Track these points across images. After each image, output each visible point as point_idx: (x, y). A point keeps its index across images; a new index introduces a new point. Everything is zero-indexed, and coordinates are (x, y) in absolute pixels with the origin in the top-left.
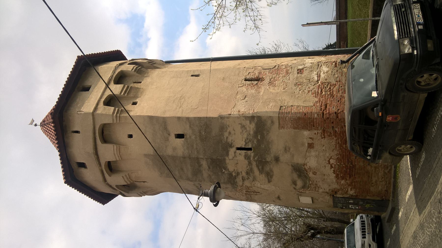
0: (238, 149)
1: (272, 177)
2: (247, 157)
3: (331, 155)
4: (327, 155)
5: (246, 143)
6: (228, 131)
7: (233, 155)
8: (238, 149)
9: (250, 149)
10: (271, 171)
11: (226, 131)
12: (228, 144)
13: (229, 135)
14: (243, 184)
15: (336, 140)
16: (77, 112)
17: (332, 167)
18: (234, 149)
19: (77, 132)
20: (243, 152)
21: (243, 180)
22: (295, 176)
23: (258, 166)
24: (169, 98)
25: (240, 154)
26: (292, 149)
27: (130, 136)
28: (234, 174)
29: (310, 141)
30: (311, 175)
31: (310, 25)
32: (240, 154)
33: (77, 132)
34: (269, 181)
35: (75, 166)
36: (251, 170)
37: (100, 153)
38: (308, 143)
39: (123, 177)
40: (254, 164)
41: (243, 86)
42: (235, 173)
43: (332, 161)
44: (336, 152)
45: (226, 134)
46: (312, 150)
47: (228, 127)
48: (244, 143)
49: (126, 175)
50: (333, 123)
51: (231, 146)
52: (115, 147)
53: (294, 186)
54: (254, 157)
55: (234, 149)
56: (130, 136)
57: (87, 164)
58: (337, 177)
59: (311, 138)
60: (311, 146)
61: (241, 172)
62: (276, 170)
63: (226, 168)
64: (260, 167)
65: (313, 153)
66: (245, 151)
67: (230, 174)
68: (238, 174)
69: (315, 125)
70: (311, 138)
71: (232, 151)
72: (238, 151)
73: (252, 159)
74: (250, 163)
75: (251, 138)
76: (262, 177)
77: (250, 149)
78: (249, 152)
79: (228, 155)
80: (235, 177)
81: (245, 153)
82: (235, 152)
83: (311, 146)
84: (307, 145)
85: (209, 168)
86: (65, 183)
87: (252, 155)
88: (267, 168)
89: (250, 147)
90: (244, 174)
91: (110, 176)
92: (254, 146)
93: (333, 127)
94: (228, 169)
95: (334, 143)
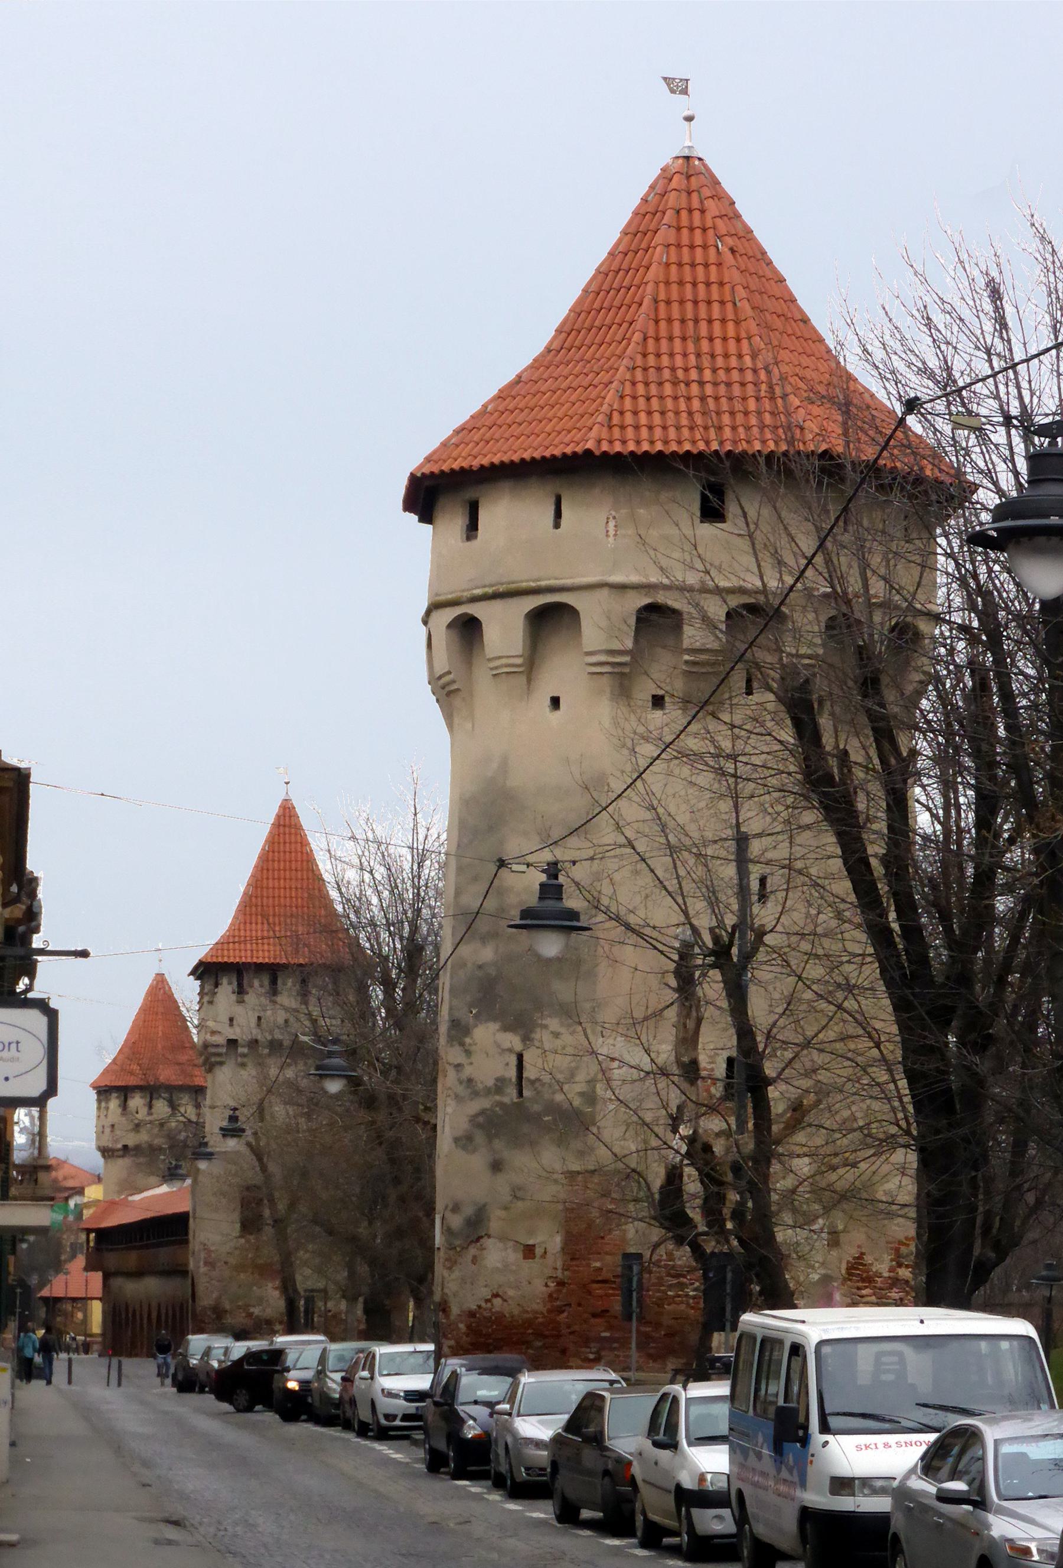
0: (520, 1057)
1: (464, 1148)
2: (500, 1084)
3: (510, 1302)
4: (511, 1293)
5: (532, 1082)
6: (562, 1030)
7: (507, 1045)
8: (520, 1057)
9: (520, 1094)
10: (474, 1151)
11: (562, 1024)
12: (531, 1032)
13: (552, 1032)
14: (450, 1064)
15: (542, 1313)
16: (614, 518)
17: (487, 1301)
18: (518, 1046)
19: (558, 514)
20: (512, 1073)
21: (458, 1067)
22: (468, 1211)
23: (483, 1112)
24: (659, 755)
25: (507, 1064)
26: (520, 1204)
27: (555, 702)
28: (468, 1040)
29: (539, 1251)
30: (472, 1251)
31: (1042, 540)
32: (507, 1064)
33: (558, 514)
34: (456, 1140)
35: (470, 494)
36: (476, 1094)
37: (497, 605)
38: (534, 1246)
39: (449, 673)
40: (485, 1103)
41: (694, 881)
42: (470, 1045)
43: (497, 1302)
44: (516, 1312)
45: (554, 1024)
46: (520, 1255)
47: (571, 1029)
48: (533, 1077)
49: (453, 682)
50: (579, 1305)
51: (526, 1039)
52: (519, 661)
53: (450, 1206)
54: (501, 1105)
55: (518, 1046)
56: (555, 702)
57: (474, 543)
58: (472, 1314)
59: (545, 1252)
60: (529, 1252)
61: (471, 1064)
62: (478, 1161)
63: (477, 1017)
64: (481, 1119)
65: (514, 1256)
66: (514, 1080)
67: (467, 1031)
68: (468, 1053)
69: (574, 1263)
70: (545, 1252)
71: (513, 1041)
72: (513, 1060)
73: (498, 1098)
74: (488, 1092)
75: (546, 1096)
76: (463, 1125)
77: (520, 1094)
78: (512, 1092)
79: (506, 1029)
80: (462, 1044)
81: (510, 1080)
82: (510, 1050)
83: (529, 1252)
84: (531, 1242)
85: (480, 967)
86: (411, 474)
87: (506, 1100)
88: (480, 1138)
89: (526, 1093)
90: (468, 1071)
91: (450, 626)
92: (546, 1453)
93: (569, 1305)
94: (476, 1026)
95: (535, 1307)
